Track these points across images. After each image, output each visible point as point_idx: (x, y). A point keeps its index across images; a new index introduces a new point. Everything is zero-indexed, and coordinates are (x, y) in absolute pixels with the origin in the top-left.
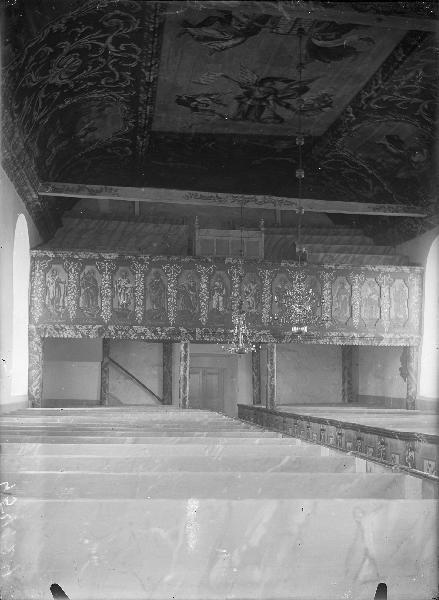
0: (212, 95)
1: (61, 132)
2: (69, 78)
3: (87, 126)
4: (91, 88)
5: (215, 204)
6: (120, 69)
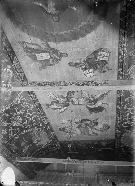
0: (69, 127)
1: (26, 142)
2: (21, 124)
3: (36, 140)
4: (31, 127)
5: (74, 164)
6: (36, 121)
